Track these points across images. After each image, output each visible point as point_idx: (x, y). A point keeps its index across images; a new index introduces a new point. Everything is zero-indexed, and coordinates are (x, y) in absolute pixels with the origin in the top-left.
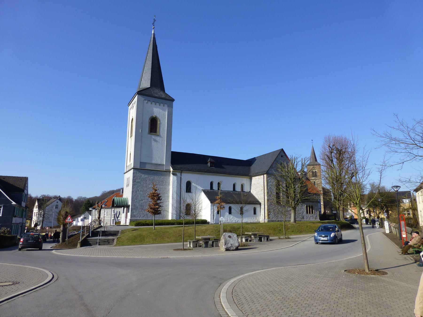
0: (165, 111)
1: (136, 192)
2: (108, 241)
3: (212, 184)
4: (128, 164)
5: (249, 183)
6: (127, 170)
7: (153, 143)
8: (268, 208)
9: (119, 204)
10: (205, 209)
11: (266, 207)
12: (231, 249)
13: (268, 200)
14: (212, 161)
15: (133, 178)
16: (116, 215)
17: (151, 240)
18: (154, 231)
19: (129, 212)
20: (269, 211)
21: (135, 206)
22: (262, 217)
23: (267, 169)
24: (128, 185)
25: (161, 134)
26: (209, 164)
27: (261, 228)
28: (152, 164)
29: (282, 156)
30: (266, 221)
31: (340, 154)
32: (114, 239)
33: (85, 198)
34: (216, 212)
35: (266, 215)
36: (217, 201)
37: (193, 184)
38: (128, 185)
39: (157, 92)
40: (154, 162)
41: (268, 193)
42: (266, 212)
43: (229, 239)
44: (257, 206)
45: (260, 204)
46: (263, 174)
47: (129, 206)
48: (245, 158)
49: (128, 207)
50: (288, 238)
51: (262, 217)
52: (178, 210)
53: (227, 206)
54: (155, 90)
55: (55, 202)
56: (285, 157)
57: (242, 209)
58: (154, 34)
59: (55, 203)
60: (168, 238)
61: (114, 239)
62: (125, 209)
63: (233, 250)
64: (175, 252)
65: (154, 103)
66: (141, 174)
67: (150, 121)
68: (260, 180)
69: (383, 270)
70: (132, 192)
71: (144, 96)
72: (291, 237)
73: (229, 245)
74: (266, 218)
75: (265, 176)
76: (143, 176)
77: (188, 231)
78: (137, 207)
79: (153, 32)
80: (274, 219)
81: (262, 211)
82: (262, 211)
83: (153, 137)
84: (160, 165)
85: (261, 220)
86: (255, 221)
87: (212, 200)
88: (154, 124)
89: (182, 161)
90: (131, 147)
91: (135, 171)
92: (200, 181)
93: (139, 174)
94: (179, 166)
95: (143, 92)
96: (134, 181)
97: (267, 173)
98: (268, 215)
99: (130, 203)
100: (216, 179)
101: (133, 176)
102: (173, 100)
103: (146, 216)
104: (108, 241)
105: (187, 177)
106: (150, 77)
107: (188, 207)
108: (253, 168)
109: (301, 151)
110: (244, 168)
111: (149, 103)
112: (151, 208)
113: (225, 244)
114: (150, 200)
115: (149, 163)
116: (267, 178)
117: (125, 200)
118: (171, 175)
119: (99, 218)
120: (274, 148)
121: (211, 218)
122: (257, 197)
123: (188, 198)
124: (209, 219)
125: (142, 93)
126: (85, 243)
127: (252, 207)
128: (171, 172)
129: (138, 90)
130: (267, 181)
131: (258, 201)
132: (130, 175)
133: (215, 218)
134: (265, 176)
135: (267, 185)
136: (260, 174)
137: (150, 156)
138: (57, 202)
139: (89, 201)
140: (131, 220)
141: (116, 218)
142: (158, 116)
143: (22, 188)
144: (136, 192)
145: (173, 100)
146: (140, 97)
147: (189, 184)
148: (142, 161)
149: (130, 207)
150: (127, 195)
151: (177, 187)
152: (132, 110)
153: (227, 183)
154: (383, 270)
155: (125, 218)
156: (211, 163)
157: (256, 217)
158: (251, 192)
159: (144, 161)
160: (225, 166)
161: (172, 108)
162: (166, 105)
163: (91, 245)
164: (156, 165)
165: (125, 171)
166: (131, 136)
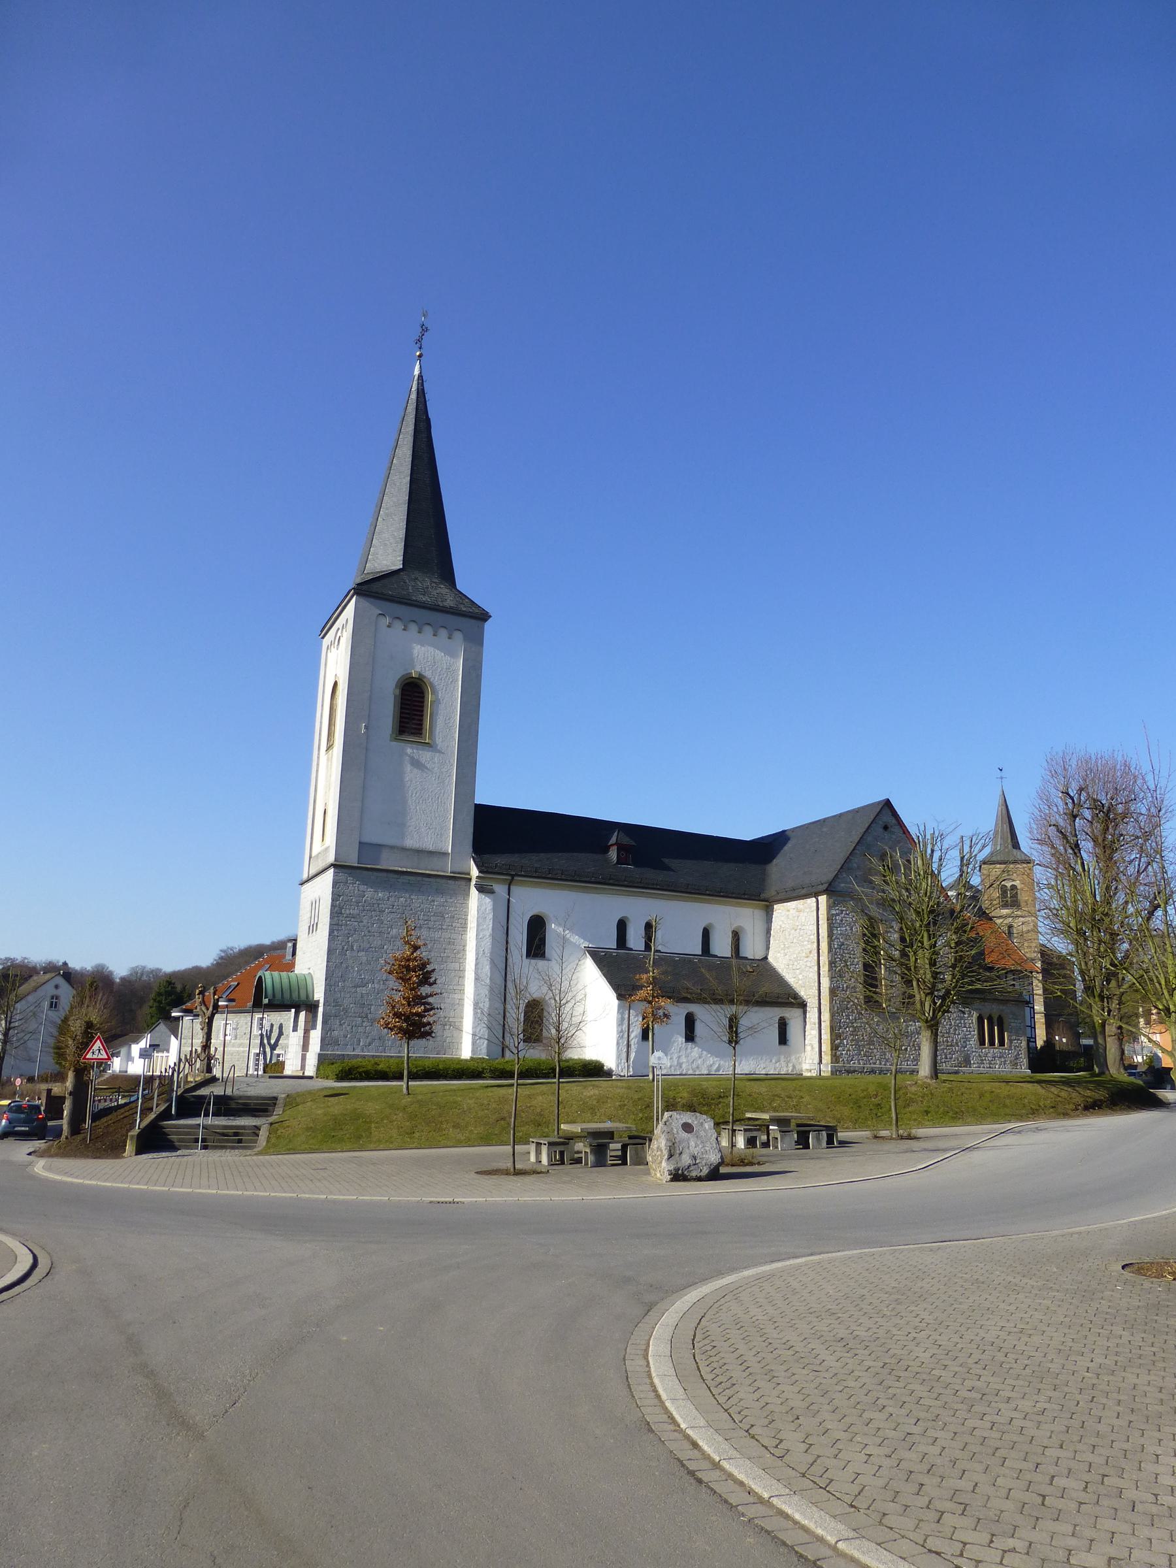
1: (343, 953)
2: (236, 1134)
3: (622, 926)
5: (760, 926)
6: (313, 872)
7: (411, 774)
10: (596, 1021)
11: (826, 1016)
12: (694, 1174)
14: (626, 840)
15: (333, 900)
16: (269, 1038)
17: (394, 1133)
19: (314, 1027)
20: (836, 1035)
21: (337, 1004)
22: (810, 1054)
23: (831, 876)
24: (313, 928)
25: (439, 740)
26: (613, 854)
28: (404, 849)
29: (886, 828)
30: (826, 1070)
32: (258, 1128)
35: (826, 1047)
37: (554, 928)
38: (313, 928)
39: (426, 586)
40: (410, 843)
41: (832, 964)
42: (826, 1036)
43: (685, 1135)
44: (792, 1015)
45: (803, 1005)
48: (747, 830)
49: (312, 1007)
53: (678, 1013)
54: (421, 582)
56: (897, 829)
58: (420, 376)
59: (49, 990)
61: (258, 1128)
62: (302, 1015)
63: (699, 1179)
65: (413, 628)
66: (362, 888)
67: (398, 692)
70: (330, 952)
72: (921, 1132)
73: (686, 1160)
74: (827, 1058)
75: (823, 899)
76: (369, 893)
77: (534, 1103)
78: (346, 1010)
79: (417, 372)
80: (855, 1064)
83: (409, 751)
84: (431, 853)
85: (805, 1066)
87: (624, 990)
88: (411, 706)
89: (513, 841)
91: (342, 876)
92: (579, 917)
93: (354, 887)
94: (500, 860)
95: (376, 587)
98: (834, 1048)
99: (319, 995)
100: (638, 908)
102: (484, 616)
103: (376, 1043)
104: (236, 1134)
105: (531, 899)
106: (402, 534)
107: (535, 1014)
108: (779, 869)
110: (742, 868)
111: (398, 625)
112: (397, 1015)
113: (671, 1156)
114: (393, 982)
115: (392, 847)
116: (829, 908)
117: (302, 983)
118: (474, 892)
121: (619, 1057)
123: (532, 978)
124: (610, 1061)
125: (372, 589)
126: (154, 1141)
127: (773, 1014)
128: (473, 882)
129: (359, 581)
131: (796, 996)
132: (323, 888)
133: (632, 1055)
134: (823, 899)
136: (803, 892)
138: (57, 987)
139: (169, 983)
140: (322, 1059)
141: (268, 1050)
142: (428, 674)
144: (343, 953)
145: (484, 616)
147: (537, 926)
148: (366, 839)
149: (321, 1009)
151: (493, 936)
153: (681, 924)
156: (621, 848)
158: (771, 959)
161: (481, 644)
162: (458, 636)
164: (420, 852)
165: (305, 876)
166: (329, 747)
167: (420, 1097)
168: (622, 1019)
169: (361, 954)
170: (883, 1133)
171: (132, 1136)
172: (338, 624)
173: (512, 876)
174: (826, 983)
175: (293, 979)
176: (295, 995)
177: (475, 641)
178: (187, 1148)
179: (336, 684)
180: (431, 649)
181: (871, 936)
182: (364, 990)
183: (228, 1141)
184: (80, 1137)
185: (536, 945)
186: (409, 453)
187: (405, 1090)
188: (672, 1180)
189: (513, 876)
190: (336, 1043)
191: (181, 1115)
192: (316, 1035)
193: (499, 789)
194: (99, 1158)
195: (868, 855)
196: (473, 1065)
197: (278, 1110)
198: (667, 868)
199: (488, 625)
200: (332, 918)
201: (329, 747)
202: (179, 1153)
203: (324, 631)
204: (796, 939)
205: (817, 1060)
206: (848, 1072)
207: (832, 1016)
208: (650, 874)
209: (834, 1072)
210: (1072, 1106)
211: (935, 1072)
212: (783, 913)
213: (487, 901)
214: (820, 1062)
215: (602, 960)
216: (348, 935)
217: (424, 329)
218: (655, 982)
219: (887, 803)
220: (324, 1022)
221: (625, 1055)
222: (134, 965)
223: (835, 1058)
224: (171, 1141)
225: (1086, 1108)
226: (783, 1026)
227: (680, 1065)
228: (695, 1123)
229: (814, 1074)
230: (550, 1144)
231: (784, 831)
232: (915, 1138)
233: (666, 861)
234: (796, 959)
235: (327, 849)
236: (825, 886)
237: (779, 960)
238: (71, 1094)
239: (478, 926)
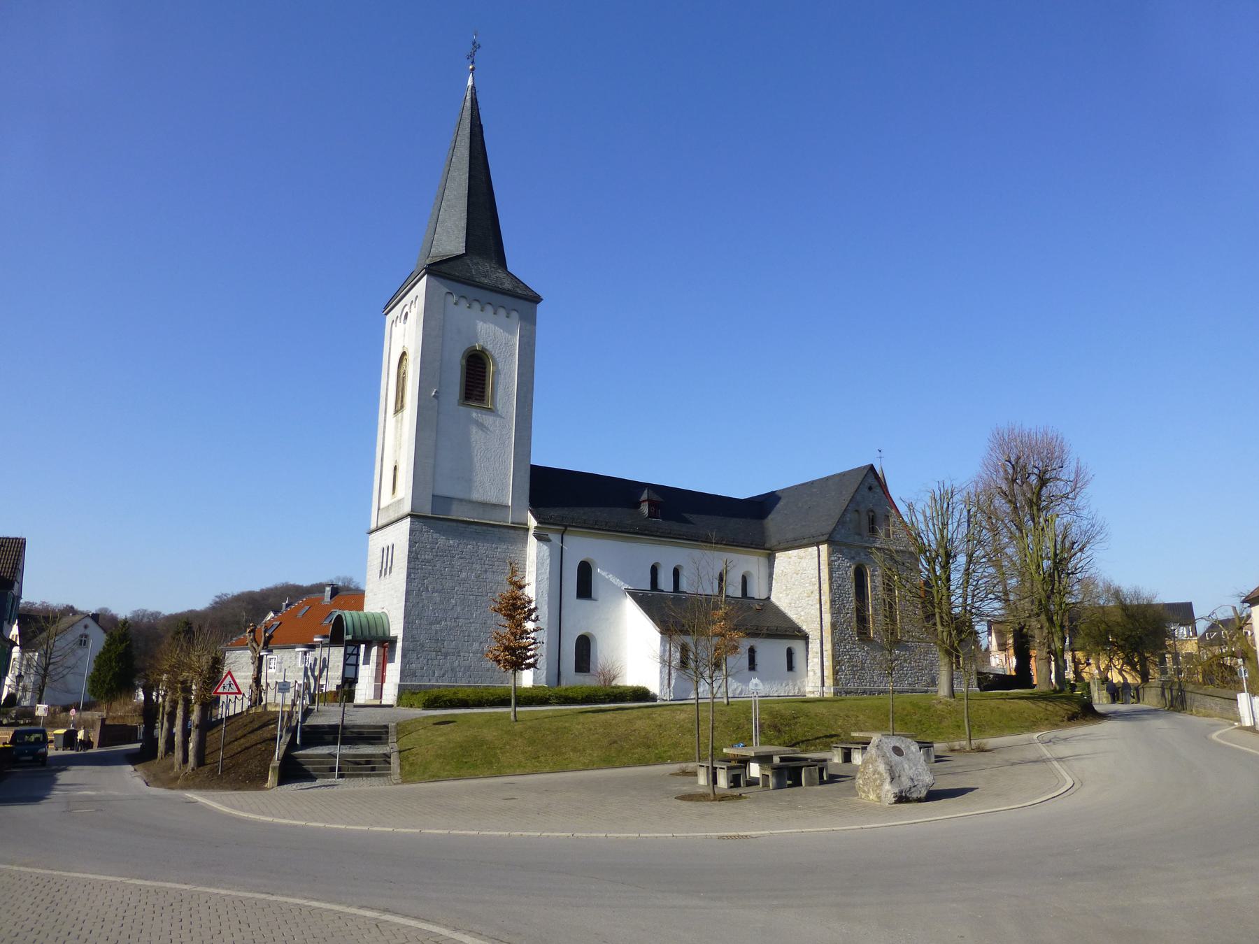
0: (512, 333)
1: (419, 593)
2: (368, 763)
3: (654, 570)
4: (387, 499)
5: (764, 572)
6: (380, 524)
7: (476, 435)
8: (833, 649)
9: (359, 632)
10: (635, 650)
11: (828, 647)
12: (915, 796)
13: (834, 626)
14: (656, 497)
15: (410, 546)
16: (313, 671)
17: (521, 758)
18: (518, 727)
19: (392, 660)
20: (836, 662)
21: (414, 639)
22: (814, 678)
23: (830, 529)
24: (385, 570)
25: (499, 407)
26: (645, 509)
27: (861, 717)
28: (471, 502)
29: (870, 488)
30: (829, 692)
31: (1030, 485)
32: (387, 756)
33: (155, 615)
35: (828, 672)
36: (716, 628)
37: (599, 572)
38: (385, 570)
39: (482, 268)
40: (476, 496)
41: (832, 602)
42: (828, 663)
43: (897, 758)
44: (798, 646)
45: (805, 638)
46: (818, 545)
47: (393, 641)
48: (742, 492)
49: (387, 644)
50: (981, 750)
51: (814, 678)
52: (359, 648)
53: (746, 644)
54: (477, 266)
55: (81, 625)
56: (878, 490)
58: (473, 87)
59: (80, 630)
60: (574, 750)
61: (387, 756)
62: (374, 650)
63: (919, 800)
64: (685, 804)
65: (476, 306)
66: (435, 535)
67: (464, 362)
68: (804, 563)
70: (408, 593)
71: (448, 282)
72: (992, 742)
73: (906, 783)
74: (829, 682)
75: (824, 548)
76: (442, 540)
77: (636, 727)
79: (470, 83)
80: (851, 686)
81: (814, 661)
82: (814, 661)
83: (474, 415)
84: (494, 506)
85: (808, 689)
86: (793, 692)
87: (667, 626)
88: (475, 375)
89: (564, 497)
90: (398, 446)
91: (418, 525)
92: (618, 561)
93: (428, 535)
94: (554, 513)
95: (444, 268)
96: (413, 557)
97: (830, 541)
98: (835, 673)
99: (396, 629)
100: (669, 555)
101: (410, 540)
102: (536, 299)
103: (449, 674)
104: (368, 763)
105: (581, 547)
106: (463, 223)
107: (584, 646)
108: (774, 523)
109: (934, 474)
110: (748, 523)
111: (464, 304)
112: (506, 648)
113: (892, 779)
114: (503, 620)
115: (461, 500)
116: (830, 555)
117: (379, 622)
118: (532, 541)
119: (257, 680)
120: (841, 459)
121: (662, 684)
122: (792, 615)
123: (580, 617)
124: (654, 687)
125: (439, 270)
126: (292, 772)
127: (781, 646)
128: (531, 532)
129: (428, 262)
130: (830, 564)
131: (799, 630)
132: (400, 536)
133: (673, 682)
134: (824, 548)
135: (831, 578)
136: (805, 542)
137: (467, 478)
138: (86, 627)
139: (187, 623)
140: (402, 689)
141: (312, 681)
142: (489, 347)
143: (7, 575)
144: (419, 593)
145: (536, 299)
146: (435, 282)
147: (585, 571)
149: (399, 645)
150: (386, 600)
151: (550, 579)
152: (400, 325)
153: (701, 568)
155: (378, 687)
156: (652, 504)
157: (794, 680)
158: (773, 599)
159: (446, 490)
160: (692, 517)
161: (535, 324)
162: (515, 315)
163: (311, 778)
164: (484, 505)
165: (373, 526)
166: (399, 407)
167: (529, 724)
168: (664, 651)
169: (436, 595)
170: (956, 745)
171: (274, 768)
173: (565, 527)
174: (827, 618)
175: (364, 620)
176: (373, 633)
177: (529, 320)
178: (324, 777)
179: (404, 354)
180: (492, 326)
181: (860, 576)
182: (438, 627)
183: (361, 769)
184: (207, 768)
185: (585, 590)
186: (467, 153)
187: (512, 718)
188: (896, 802)
189: (566, 526)
190: (414, 674)
191: (305, 745)
192: (393, 671)
193: (551, 453)
194: (239, 789)
195: (856, 515)
196: (535, 693)
197: (392, 738)
198: (686, 521)
199: (540, 307)
200: (409, 562)
201: (399, 407)
202: (319, 782)
203: (388, 308)
204: (799, 582)
205: (819, 684)
206: (847, 693)
207: (833, 645)
208: (676, 526)
209: (835, 694)
210: (1059, 718)
211: (952, 694)
212: (784, 561)
213: (545, 548)
214: (823, 685)
215: (643, 600)
216: (424, 578)
217: (476, 46)
218: (726, 617)
219: (872, 468)
220: (403, 656)
221: (666, 682)
222: (136, 609)
223: (836, 681)
224: (305, 770)
225: (1070, 719)
226: (790, 653)
227: (246, 678)
228: (903, 747)
229: (817, 695)
230: (729, 768)
231: (773, 493)
234: (798, 599)
235: (400, 501)
236: (826, 537)
237: (782, 599)
238: (197, 727)
239: (537, 570)
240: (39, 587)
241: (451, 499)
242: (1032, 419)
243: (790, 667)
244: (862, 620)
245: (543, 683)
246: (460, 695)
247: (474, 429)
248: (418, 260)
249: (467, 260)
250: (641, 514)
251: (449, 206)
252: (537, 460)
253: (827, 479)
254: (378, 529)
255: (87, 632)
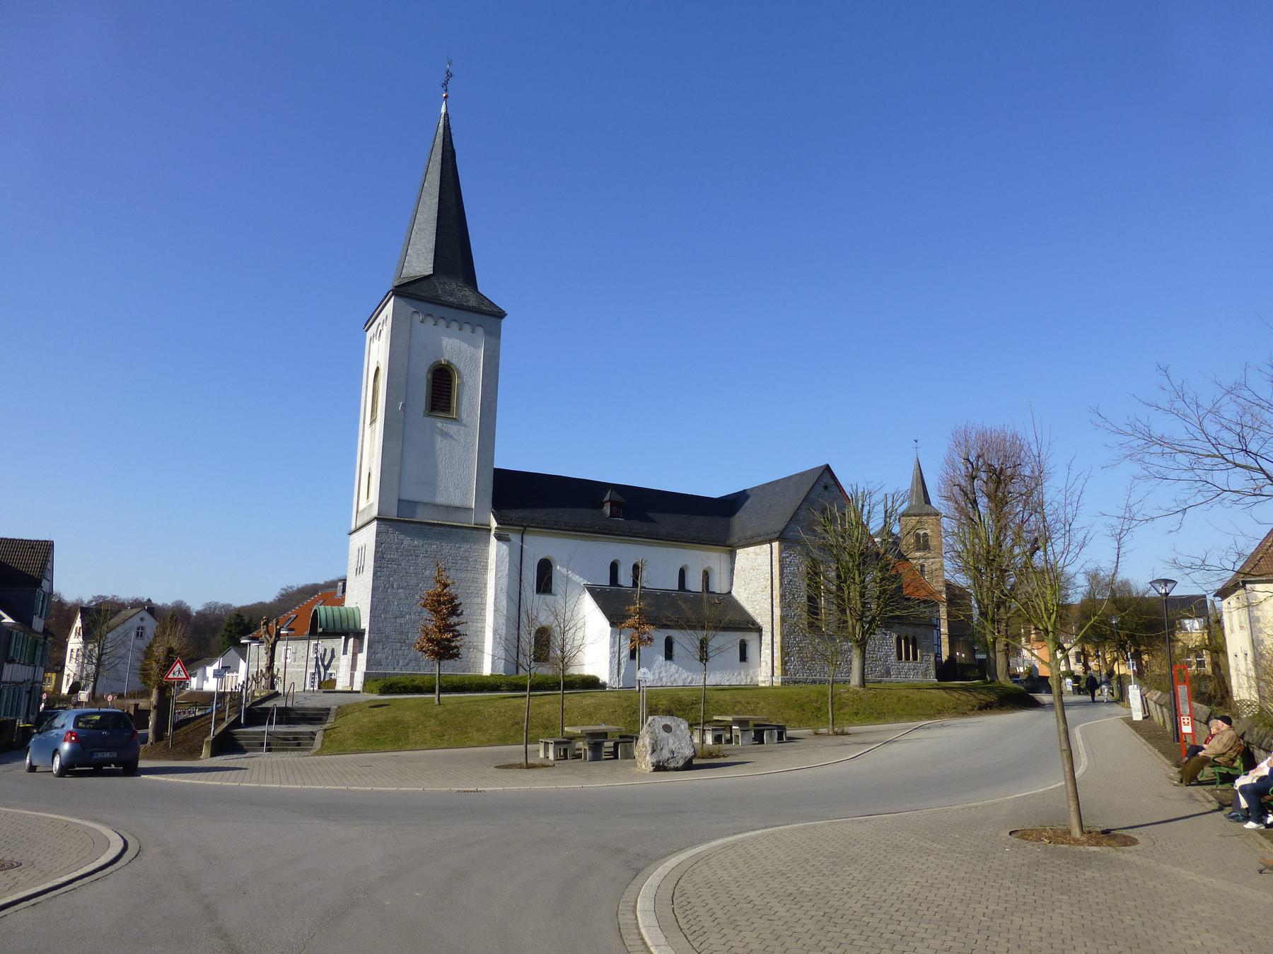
0: (476, 346)
1: (385, 590)
2: (295, 739)
3: (614, 567)
5: (725, 566)
6: (359, 524)
7: (440, 444)
8: (782, 642)
11: (777, 639)
12: (672, 765)
13: (783, 619)
14: (618, 498)
16: (323, 661)
17: (428, 736)
19: (361, 651)
20: (785, 653)
22: (765, 669)
24: (359, 570)
25: (464, 416)
26: (607, 509)
29: (826, 488)
30: (777, 681)
31: (997, 480)
33: (226, 608)
34: (625, 652)
35: (777, 663)
37: (558, 569)
38: (359, 570)
39: (453, 289)
40: (440, 500)
41: (783, 597)
42: (777, 654)
44: (751, 638)
45: (759, 630)
46: (770, 542)
48: (716, 493)
49: (359, 635)
50: (843, 734)
54: (448, 284)
56: (835, 489)
57: (703, 644)
58: (446, 114)
59: (136, 621)
62: (351, 641)
63: (677, 769)
64: (502, 772)
65: (442, 323)
66: (401, 537)
67: (430, 376)
69: (1125, 832)
72: (852, 729)
73: (666, 754)
74: (778, 672)
75: (776, 545)
76: (407, 541)
79: (443, 110)
80: (799, 676)
81: (766, 652)
82: (766, 652)
83: (439, 425)
84: (458, 508)
85: (761, 679)
87: (615, 619)
89: (525, 499)
90: (372, 454)
91: (384, 528)
92: (579, 560)
93: (394, 537)
94: (514, 514)
95: (410, 289)
96: (379, 557)
98: (784, 663)
99: (365, 624)
100: (627, 553)
102: (501, 315)
103: (413, 663)
104: (295, 739)
105: (540, 546)
106: (432, 245)
107: (543, 638)
108: (741, 521)
110: (710, 521)
111: (430, 321)
113: (653, 751)
114: (426, 614)
116: (781, 552)
117: (351, 616)
118: (493, 540)
121: (611, 673)
122: (749, 608)
123: (541, 610)
124: (604, 677)
125: (407, 291)
126: (226, 744)
129: (396, 284)
130: (781, 561)
131: (754, 623)
132: (368, 537)
133: (622, 671)
134: (776, 545)
135: (781, 574)
138: (142, 619)
140: (367, 676)
141: (322, 670)
142: (455, 361)
143: (36, 574)
144: (385, 590)
145: (501, 315)
146: (402, 302)
147: (545, 569)
149: (366, 636)
150: (359, 598)
152: (376, 341)
153: (661, 565)
154: (1125, 832)
155: (349, 670)
161: (499, 337)
162: (480, 330)
163: (244, 752)
164: (449, 508)
165: (353, 528)
166: (373, 421)
168: (614, 642)
172: (380, 319)
174: (777, 611)
175: (344, 615)
179: (378, 369)
196: (492, 681)
198: (651, 520)
199: (504, 321)
201: (373, 421)
203: (368, 324)
204: (753, 577)
206: (795, 682)
208: (636, 525)
211: (863, 682)
213: (505, 547)
215: (601, 597)
219: (827, 468)
220: (369, 647)
225: (981, 709)
227: (661, 679)
228: (673, 725)
229: (767, 684)
232: (847, 734)
233: (650, 514)
234: (755, 593)
240: (72, 582)
241: (416, 503)
242: (1004, 412)
243: (743, 657)
244: (813, 609)
245: (501, 671)
246: (417, 682)
247: (438, 439)
248: (391, 283)
249: (434, 280)
250: (603, 514)
251: (420, 229)
252: (500, 463)
253: (790, 477)
254: (355, 531)
255: (143, 624)
